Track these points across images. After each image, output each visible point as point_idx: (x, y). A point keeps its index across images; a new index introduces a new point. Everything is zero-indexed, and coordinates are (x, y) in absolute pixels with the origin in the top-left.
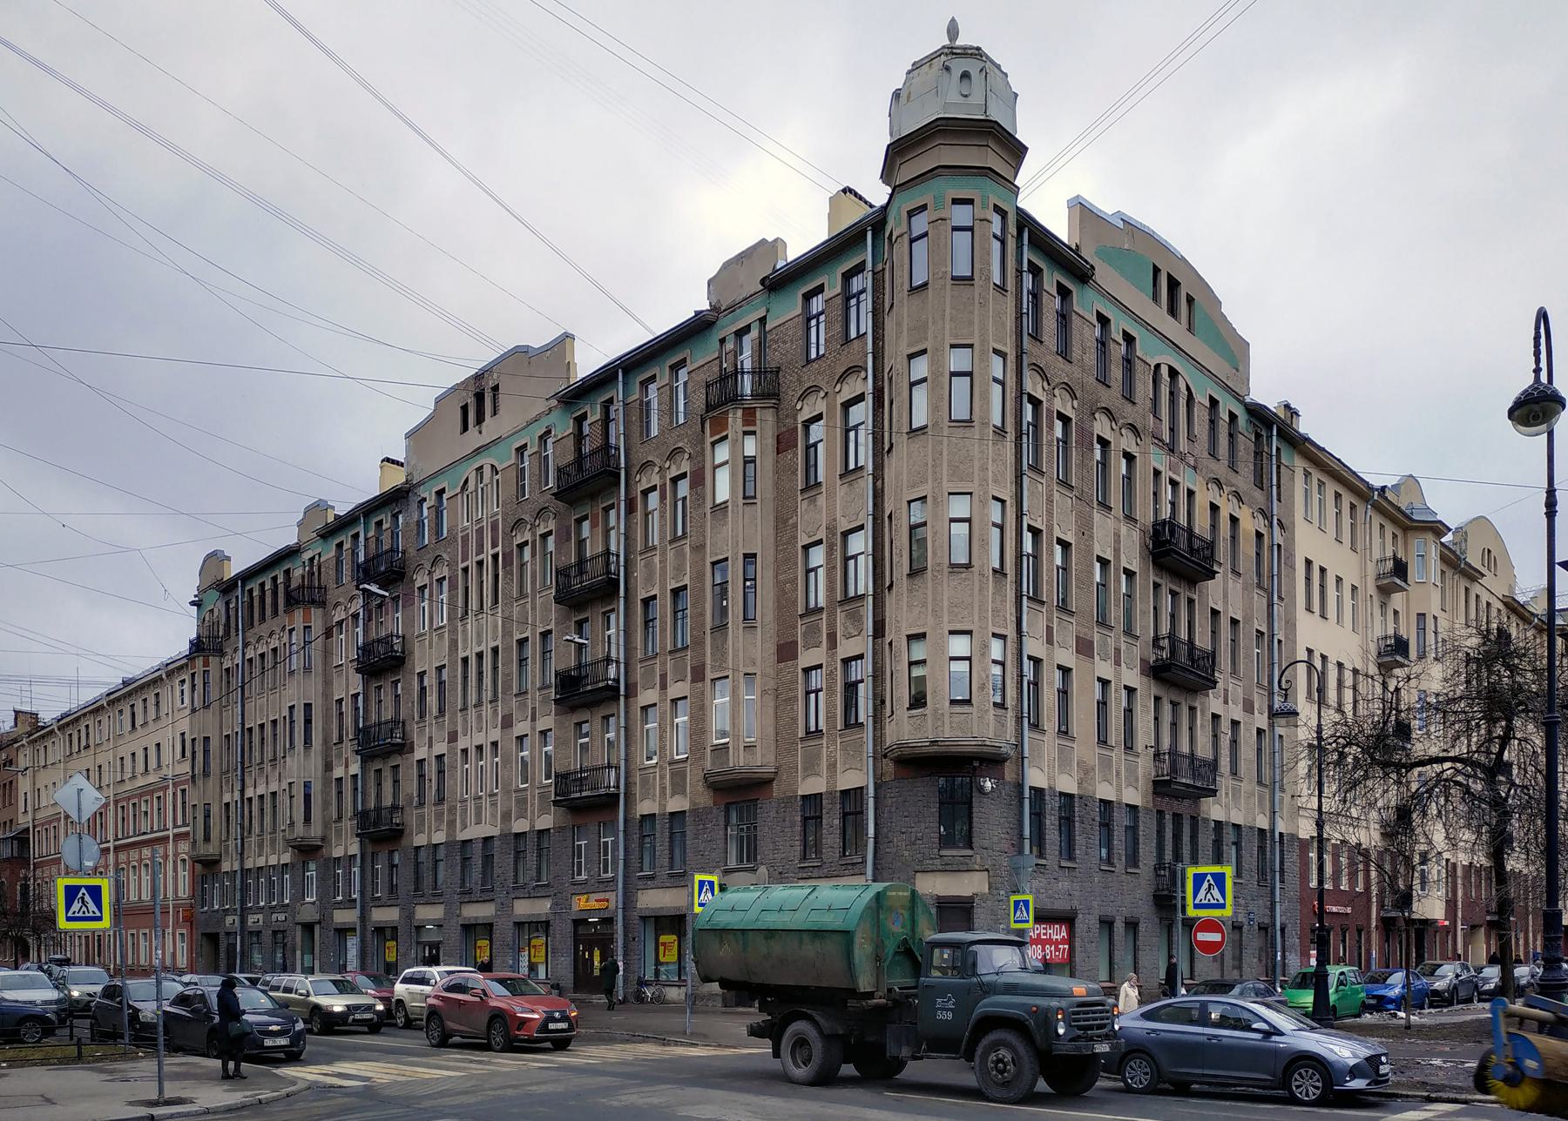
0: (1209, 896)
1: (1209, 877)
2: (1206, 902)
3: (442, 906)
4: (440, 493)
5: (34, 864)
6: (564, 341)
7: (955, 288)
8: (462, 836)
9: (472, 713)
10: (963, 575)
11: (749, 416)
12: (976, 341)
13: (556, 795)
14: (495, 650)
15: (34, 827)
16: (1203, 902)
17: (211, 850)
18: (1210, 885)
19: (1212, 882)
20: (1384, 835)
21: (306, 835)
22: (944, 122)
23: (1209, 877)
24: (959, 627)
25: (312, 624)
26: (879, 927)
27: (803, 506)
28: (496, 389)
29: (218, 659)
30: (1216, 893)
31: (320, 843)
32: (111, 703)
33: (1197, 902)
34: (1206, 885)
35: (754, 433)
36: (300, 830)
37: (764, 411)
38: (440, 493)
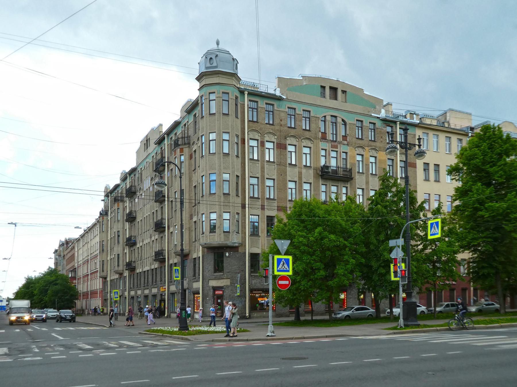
0: (283, 267)
1: (283, 260)
2: (282, 269)
3: (134, 291)
4: (141, 169)
5: (78, 279)
6: (161, 125)
7: (210, 117)
8: (144, 270)
9: (146, 233)
10: (213, 196)
11: (182, 150)
12: (216, 131)
13: (155, 258)
14: (149, 215)
15: (78, 267)
16: (281, 269)
17: (104, 274)
18: (284, 263)
19: (284, 262)
20: (230, 283)
21: (118, 270)
22: (204, 73)
23: (283, 260)
24: (212, 211)
25: (120, 207)
26: (41, 364)
27: (194, 175)
28: (149, 139)
29: (106, 217)
30: (286, 266)
31: (122, 272)
32: (89, 230)
33: (279, 269)
34: (282, 263)
35: (183, 155)
36: (116, 268)
37: (186, 148)
38: (141, 169)
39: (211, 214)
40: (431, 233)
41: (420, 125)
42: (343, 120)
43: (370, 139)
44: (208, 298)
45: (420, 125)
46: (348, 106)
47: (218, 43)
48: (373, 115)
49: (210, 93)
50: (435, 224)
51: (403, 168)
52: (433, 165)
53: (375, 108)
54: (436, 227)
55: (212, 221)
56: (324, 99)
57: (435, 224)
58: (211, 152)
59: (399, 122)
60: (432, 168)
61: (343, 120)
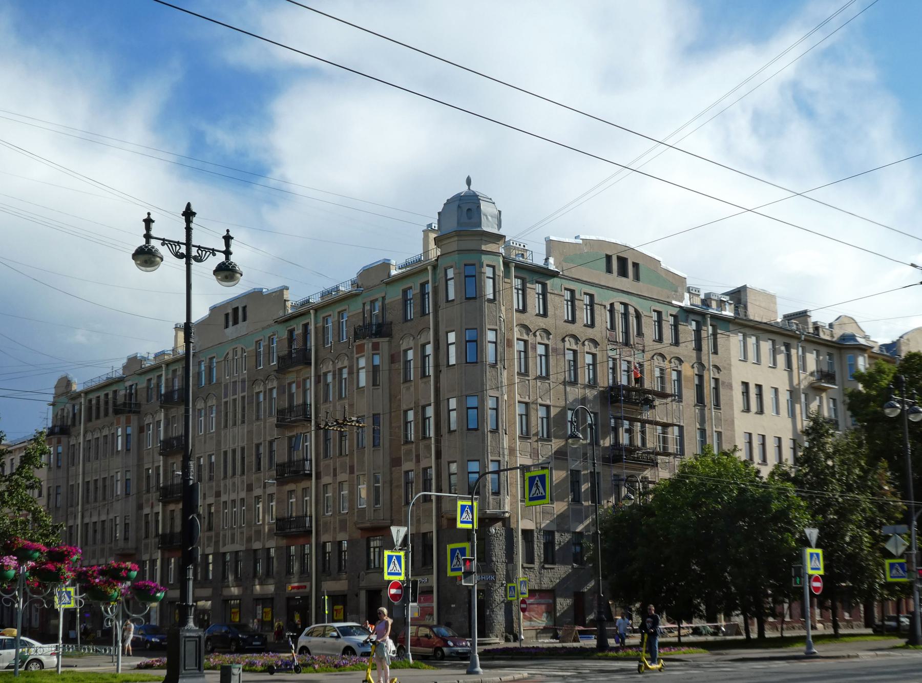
39: (470, 463)
40: (531, 496)
41: (736, 320)
42: (636, 311)
43: (566, 318)
44: (453, 606)
45: (736, 320)
46: (640, 288)
47: (469, 182)
48: (674, 302)
49: (465, 265)
50: (537, 479)
51: (676, 382)
52: (754, 386)
53: (676, 291)
54: (539, 484)
55: (471, 475)
56: (624, 279)
57: (537, 479)
58: (468, 361)
59: (709, 316)
60: (753, 391)
61: (636, 311)
